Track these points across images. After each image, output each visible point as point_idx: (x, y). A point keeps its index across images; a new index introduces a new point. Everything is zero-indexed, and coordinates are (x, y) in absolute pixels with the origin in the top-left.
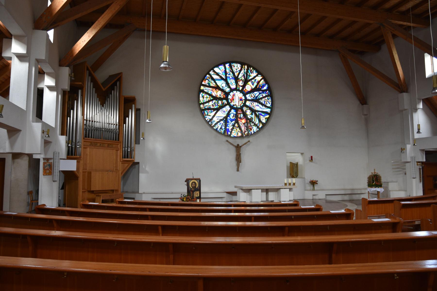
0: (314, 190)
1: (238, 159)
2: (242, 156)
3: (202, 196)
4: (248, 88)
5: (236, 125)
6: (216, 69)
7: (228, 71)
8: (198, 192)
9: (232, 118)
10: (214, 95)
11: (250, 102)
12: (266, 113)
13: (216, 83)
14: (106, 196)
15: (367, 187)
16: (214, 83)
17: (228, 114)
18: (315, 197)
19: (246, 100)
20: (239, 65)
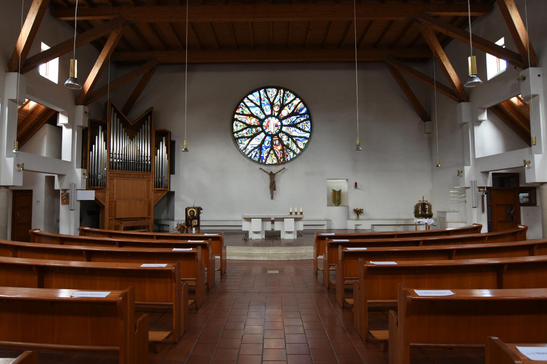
0: (358, 219)
1: (273, 187)
2: (277, 184)
3: (202, 223)
4: (284, 113)
5: (272, 152)
6: (250, 97)
7: (262, 97)
8: (196, 221)
9: (266, 145)
10: (248, 123)
11: (286, 128)
12: (305, 138)
13: (250, 111)
14: (130, 224)
15: (413, 216)
16: (248, 111)
17: (263, 142)
18: (359, 228)
19: (282, 125)
20: (274, 90)
